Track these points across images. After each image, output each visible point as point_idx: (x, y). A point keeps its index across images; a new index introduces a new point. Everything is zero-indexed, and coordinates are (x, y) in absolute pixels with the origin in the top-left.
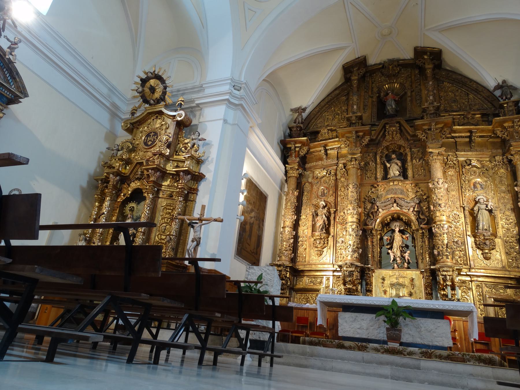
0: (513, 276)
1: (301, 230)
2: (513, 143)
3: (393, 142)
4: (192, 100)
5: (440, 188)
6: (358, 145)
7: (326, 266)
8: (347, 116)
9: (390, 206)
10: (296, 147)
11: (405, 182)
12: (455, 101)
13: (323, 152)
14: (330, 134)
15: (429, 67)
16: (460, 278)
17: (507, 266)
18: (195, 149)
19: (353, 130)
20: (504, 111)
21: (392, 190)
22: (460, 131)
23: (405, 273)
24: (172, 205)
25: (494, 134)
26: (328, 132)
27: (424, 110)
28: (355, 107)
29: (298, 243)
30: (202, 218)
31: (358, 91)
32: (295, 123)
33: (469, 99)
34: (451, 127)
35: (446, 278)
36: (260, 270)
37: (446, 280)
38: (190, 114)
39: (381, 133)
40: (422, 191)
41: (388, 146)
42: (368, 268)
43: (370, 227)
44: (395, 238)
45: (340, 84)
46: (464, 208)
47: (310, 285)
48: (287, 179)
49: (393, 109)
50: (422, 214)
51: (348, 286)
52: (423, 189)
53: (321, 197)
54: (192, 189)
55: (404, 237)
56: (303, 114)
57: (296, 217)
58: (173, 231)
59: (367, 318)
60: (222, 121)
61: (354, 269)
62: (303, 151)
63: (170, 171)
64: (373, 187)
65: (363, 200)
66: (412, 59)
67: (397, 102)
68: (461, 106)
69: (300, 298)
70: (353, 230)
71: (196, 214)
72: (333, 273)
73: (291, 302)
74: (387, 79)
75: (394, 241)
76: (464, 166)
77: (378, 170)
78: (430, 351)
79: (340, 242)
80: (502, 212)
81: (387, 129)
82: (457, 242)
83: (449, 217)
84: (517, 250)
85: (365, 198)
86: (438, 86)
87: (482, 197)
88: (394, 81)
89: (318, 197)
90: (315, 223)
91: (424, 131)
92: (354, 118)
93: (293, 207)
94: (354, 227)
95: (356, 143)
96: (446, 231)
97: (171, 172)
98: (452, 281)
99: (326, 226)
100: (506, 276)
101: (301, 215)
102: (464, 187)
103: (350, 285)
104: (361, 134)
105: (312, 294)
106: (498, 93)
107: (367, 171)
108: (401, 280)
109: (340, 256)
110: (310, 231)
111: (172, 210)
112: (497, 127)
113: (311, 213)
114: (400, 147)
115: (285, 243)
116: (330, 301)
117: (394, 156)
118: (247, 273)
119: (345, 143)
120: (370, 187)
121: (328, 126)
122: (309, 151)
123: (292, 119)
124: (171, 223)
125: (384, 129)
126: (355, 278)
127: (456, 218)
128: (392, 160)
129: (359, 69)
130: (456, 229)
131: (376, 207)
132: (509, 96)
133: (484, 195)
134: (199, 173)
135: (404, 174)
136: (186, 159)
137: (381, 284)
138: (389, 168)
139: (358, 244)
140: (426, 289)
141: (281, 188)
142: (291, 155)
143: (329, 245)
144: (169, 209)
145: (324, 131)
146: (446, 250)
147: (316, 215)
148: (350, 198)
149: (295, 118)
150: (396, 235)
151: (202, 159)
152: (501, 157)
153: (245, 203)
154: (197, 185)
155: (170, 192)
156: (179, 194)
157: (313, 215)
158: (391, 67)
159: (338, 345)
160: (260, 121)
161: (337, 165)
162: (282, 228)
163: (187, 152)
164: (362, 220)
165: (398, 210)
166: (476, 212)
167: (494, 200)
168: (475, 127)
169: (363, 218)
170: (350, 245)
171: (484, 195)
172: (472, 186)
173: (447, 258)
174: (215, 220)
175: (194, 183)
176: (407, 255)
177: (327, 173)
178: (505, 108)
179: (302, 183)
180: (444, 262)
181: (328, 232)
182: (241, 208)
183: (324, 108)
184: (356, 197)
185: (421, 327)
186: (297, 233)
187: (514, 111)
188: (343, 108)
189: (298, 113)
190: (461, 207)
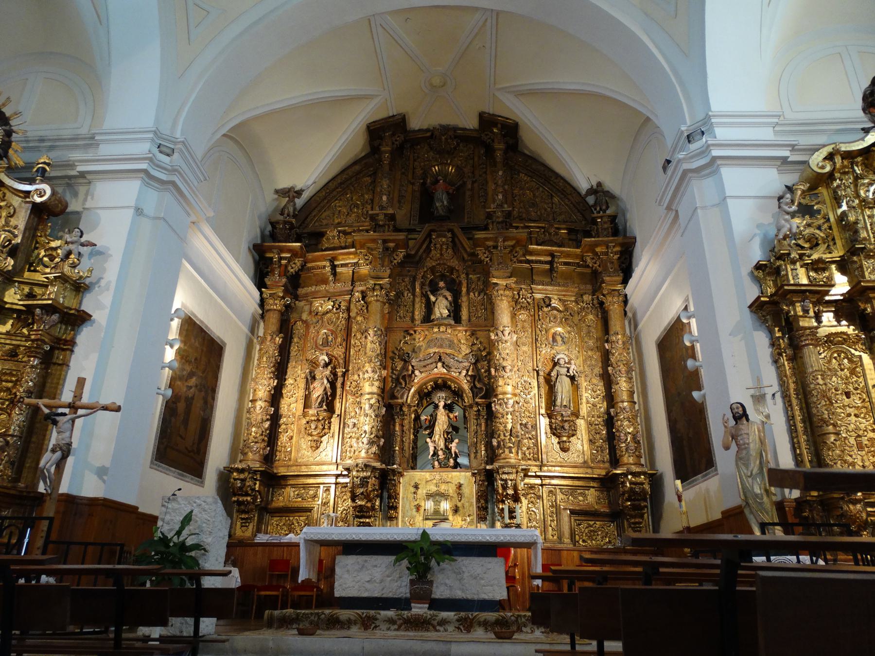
0: (596, 476)
1: (284, 404)
2: (607, 279)
3: (441, 262)
4: (71, 163)
5: (506, 341)
6: (386, 263)
7: (325, 467)
8: (370, 212)
9: (432, 366)
10: (281, 258)
11: (456, 327)
12: (534, 205)
13: (328, 269)
14: (343, 239)
15: (500, 146)
16: (527, 480)
17: (589, 461)
18: (71, 262)
19: (379, 237)
20: (597, 230)
21: (436, 341)
22: (538, 253)
23: (450, 476)
24: (14, 373)
25: (583, 261)
26: (339, 235)
27: (489, 216)
28: (384, 198)
29: (280, 426)
30: (78, 403)
31: (391, 170)
32: (282, 214)
33: (553, 203)
34: (525, 247)
35: (506, 483)
36: (189, 503)
37: (507, 487)
38: (64, 191)
39: (424, 246)
40: (481, 343)
41: (433, 266)
42: (393, 470)
43: (400, 401)
44: (438, 417)
45: (363, 154)
46: (538, 372)
47: (296, 502)
48: (263, 313)
49: (444, 206)
50: (480, 381)
51: (359, 503)
52: (482, 340)
53: (321, 347)
54: (62, 342)
55: (451, 416)
56: (296, 200)
57: (276, 381)
58: (13, 427)
59: (381, 564)
60: (131, 212)
61: (369, 474)
62: (293, 266)
63: (12, 304)
64: (408, 334)
65: (391, 354)
66: (475, 130)
67: (452, 197)
68: (541, 214)
69: (277, 525)
70: (371, 406)
71: (67, 396)
72: (337, 478)
73: (260, 533)
74: (438, 156)
75: (437, 423)
76: (542, 307)
77: (417, 306)
78: (472, 615)
79: (351, 425)
80: (588, 379)
81: (434, 239)
82: (525, 425)
83: (515, 387)
84: (603, 436)
85: (393, 352)
86: (512, 178)
87: (562, 357)
88: (447, 161)
89: (317, 347)
90: (310, 393)
91: (487, 248)
92: (381, 217)
93: (272, 365)
94: (373, 401)
95: (381, 259)
96: (511, 410)
97: (15, 307)
98: (515, 488)
99: (327, 398)
100: (587, 476)
101: (287, 377)
102: (539, 339)
103: (363, 500)
104: (392, 245)
105: (299, 516)
106: (591, 200)
107: (399, 306)
108: (443, 488)
109: (349, 449)
110: (301, 407)
111: (15, 383)
112: (587, 252)
113: (303, 376)
114: (452, 270)
115: (254, 429)
116: (323, 539)
117: (442, 284)
118: (164, 509)
119: (366, 257)
120: (402, 334)
121: (339, 224)
122: (305, 265)
123: (277, 206)
124: (11, 411)
125: (428, 239)
126: (370, 489)
127: (527, 387)
128: (438, 290)
129: (393, 135)
130: (525, 405)
131: (410, 367)
132: (604, 207)
133: (566, 353)
134: (78, 311)
135: (455, 315)
136: (51, 282)
137: (412, 496)
138: (434, 303)
139: (379, 430)
140: (478, 501)
141: (253, 329)
142: (273, 271)
143: (332, 431)
144: (7, 381)
145: (332, 233)
146: (510, 439)
147: (311, 378)
148: (369, 353)
149: (282, 207)
150: (439, 414)
151: (87, 283)
152: (590, 297)
153: (176, 365)
154: (72, 332)
155: (11, 347)
156: (32, 352)
157: (307, 379)
158: (443, 138)
159: (329, 620)
160: (211, 214)
161: (351, 294)
162: (251, 401)
163: (53, 267)
164: (388, 388)
165: (444, 374)
166: (553, 379)
167: (578, 362)
168: (558, 249)
169: (390, 384)
170: (365, 432)
171: (566, 353)
172: (551, 339)
173: (511, 452)
174: (105, 408)
175: (66, 329)
176: (453, 446)
177: (333, 307)
178: (599, 224)
179: (290, 321)
180: (505, 459)
181: (331, 409)
182: (169, 374)
183: (335, 193)
184: (378, 352)
185: (463, 572)
186: (277, 409)
187: (610, 230)
188: (366, 196)
189: (287, 199)
190: (534, 370)
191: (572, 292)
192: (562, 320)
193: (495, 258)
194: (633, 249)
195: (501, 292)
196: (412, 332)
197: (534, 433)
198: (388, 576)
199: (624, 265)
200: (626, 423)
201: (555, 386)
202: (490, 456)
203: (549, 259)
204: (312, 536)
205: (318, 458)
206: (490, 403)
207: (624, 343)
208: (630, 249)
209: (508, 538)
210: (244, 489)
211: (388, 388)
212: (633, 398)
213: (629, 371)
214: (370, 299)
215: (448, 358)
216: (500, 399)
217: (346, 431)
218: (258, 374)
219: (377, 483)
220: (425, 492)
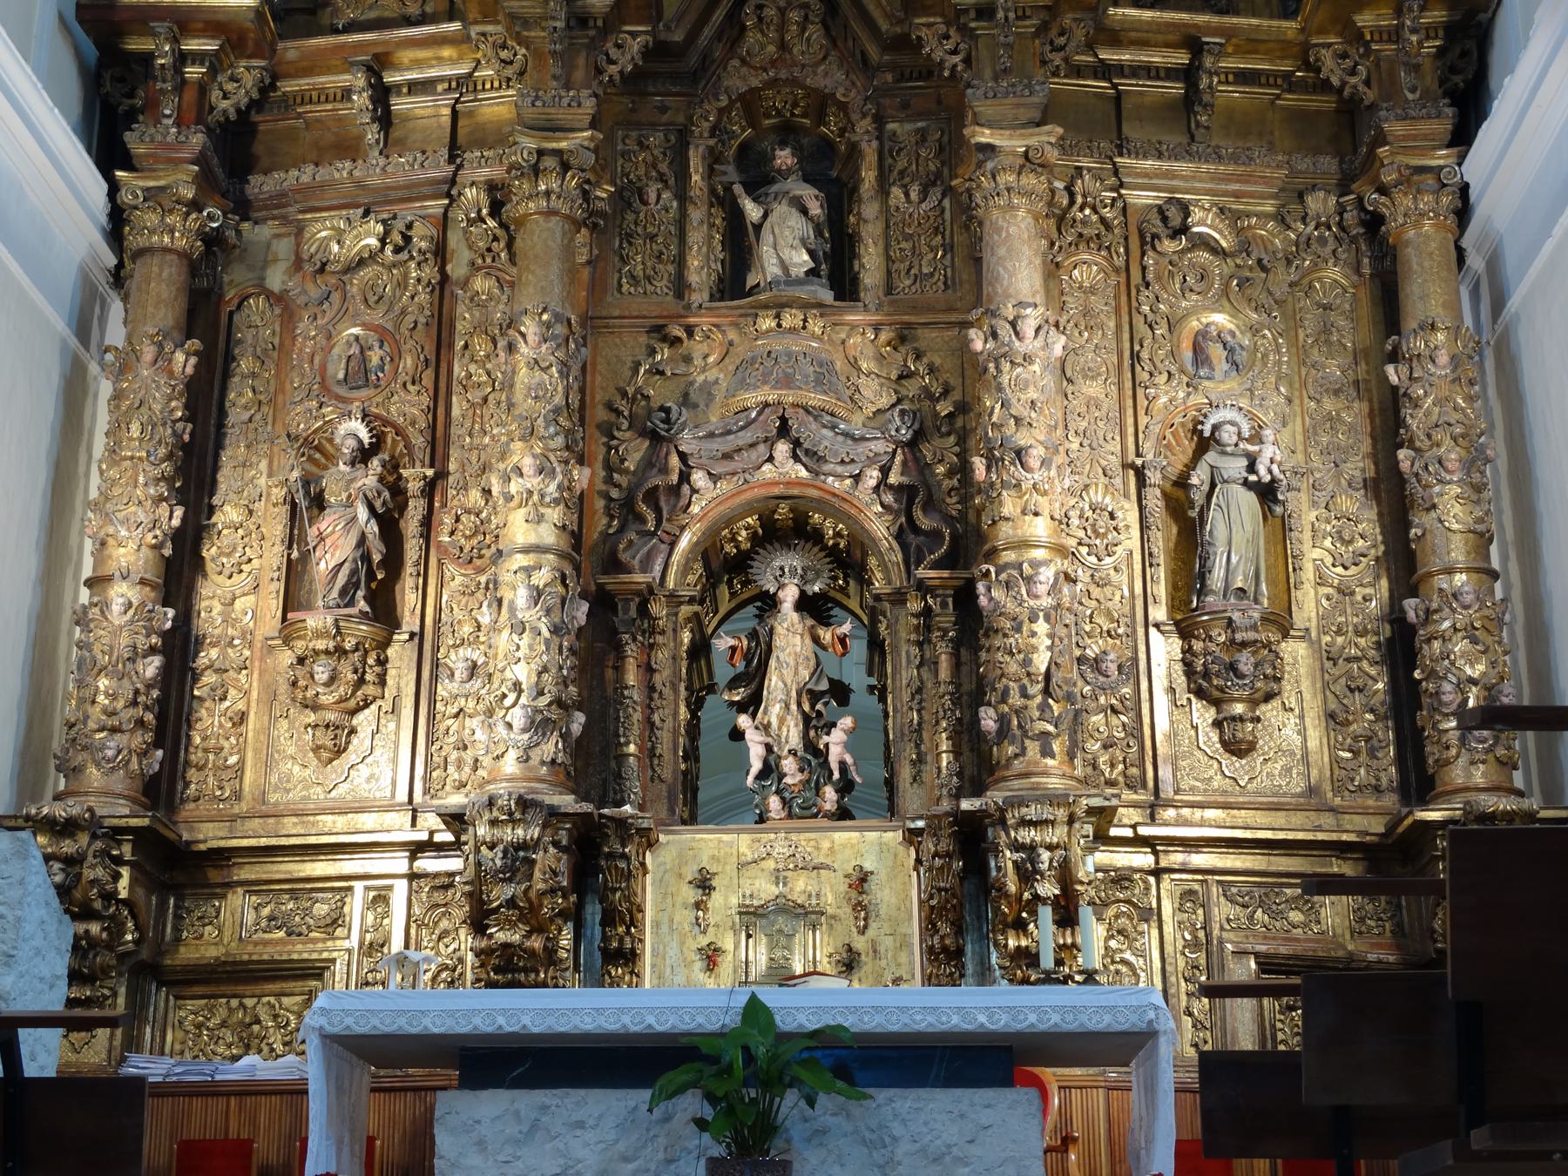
3: (783, 75)
5: (1027, 358)
6: (579, 75)
7: (367, 820)
10: (182, 58)
11: (841, 311)
13: (361, 100)
16: (1103, 857)
17: (1327, 787)
21: (769, 363)
23: (826, 845)
25: (1307, 65)
29: (196, 678)
35: (1033, 859)
37: (1036, 871)
40: (932, 370)
41: (752, 91)
42: (621, 823)
43: (639, 578)
44: (778, 642)
47: (266, 943)
48: (120, 265)
50: (928, 506)
51: (501, 936)
52: (938, 361)
53: (342, 391)
55: (826, 635)
57: (179, 512)
62: (230, 87)
64: (664, 339)
65: (602, 414)
69: (199, 1026)
70: (537, 595)
72: (413, 858)
75: (773, 663)
76: (1155, 236)
77: (695, 237)
80: (1322, 497)
82: (1097, 664)
84: (1375, 701)
85: (610, 407)
87: (1229, 419)
89: (325, 390)
90: (305, 556)
93: (162, 451)
94: (542, 577)
96: (1046, 602)
99: (371, 575)
100: (1321, 836)
101: (216, 501)
102: (1145, 355)
103: (513, 925)
105: (279, 995)
108: (800, 886)
109: (454, 755)
110: (274, 605)
112: (1322, 31)
113: (279, 493)
114: (821, 103)
115: (103, 683)
117: (784, 158)
119: (504, 54)
120: (643, 339)
122: (273, 87)
126: (541, 886)
127: (1100, 526)
128: (773, 181)
130: (1096, 592)
131: (674, 461)
133: (1244, 403)
137: (690, 915)
138: (758, 228)
140: (929, 926)
141: (85, 325)
143: (389, 692)
146: (1044, 707)
148: (525, 404)
152: (1333, 200)
157: (294, 505)
161: (448, 195)
162: (90, 583)
164: (593, 535)
165: (799, 483)
166: (1198, 497)
167: (1285, 437)
168: (1215, 19)
169: (599, 523)
170: (517, 687)
171: (1244, 403)
172: (1188, 355)
173: (1047, 752)
176: (835, 743)
177: (383, 241)
179: (221, 296)
180: (1027, 775)
181: (384, 612)
184: (558, 399)
185: (895, 1139)
186: (185, 617)
190: (1126, 466)
191: (1266, 181)
192: (1227, 285)
193: (983, 53)
194: (1492, 20)
195: (1008, 178)
196: (678, 332)
197: (1126, 690)
198: (626, 1159)
199: (1458, 79)
200: (1460, 646)
201: (1203, 522)
202: (967, 772)
203: (1182, 58)
204: (349, 1021)
205: (342, 790)
206: (970, 585)
207: (1455, 360)
208: (1483, 17)
209: (1055, 1018)
210: (77, 894)
211: (593, 535)
212: (1487, 558)
213: (1475, 460)
214: (525, 206)
215: (814, 426)
216: (1006, 566)
217: (441, 691)
218: (114, 482)
219: (563, 866)
220: (734, 901)
